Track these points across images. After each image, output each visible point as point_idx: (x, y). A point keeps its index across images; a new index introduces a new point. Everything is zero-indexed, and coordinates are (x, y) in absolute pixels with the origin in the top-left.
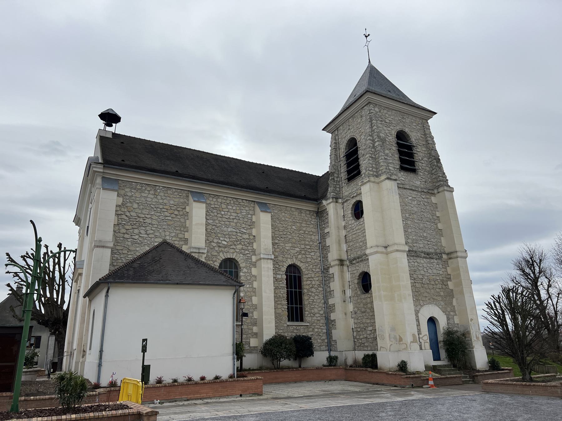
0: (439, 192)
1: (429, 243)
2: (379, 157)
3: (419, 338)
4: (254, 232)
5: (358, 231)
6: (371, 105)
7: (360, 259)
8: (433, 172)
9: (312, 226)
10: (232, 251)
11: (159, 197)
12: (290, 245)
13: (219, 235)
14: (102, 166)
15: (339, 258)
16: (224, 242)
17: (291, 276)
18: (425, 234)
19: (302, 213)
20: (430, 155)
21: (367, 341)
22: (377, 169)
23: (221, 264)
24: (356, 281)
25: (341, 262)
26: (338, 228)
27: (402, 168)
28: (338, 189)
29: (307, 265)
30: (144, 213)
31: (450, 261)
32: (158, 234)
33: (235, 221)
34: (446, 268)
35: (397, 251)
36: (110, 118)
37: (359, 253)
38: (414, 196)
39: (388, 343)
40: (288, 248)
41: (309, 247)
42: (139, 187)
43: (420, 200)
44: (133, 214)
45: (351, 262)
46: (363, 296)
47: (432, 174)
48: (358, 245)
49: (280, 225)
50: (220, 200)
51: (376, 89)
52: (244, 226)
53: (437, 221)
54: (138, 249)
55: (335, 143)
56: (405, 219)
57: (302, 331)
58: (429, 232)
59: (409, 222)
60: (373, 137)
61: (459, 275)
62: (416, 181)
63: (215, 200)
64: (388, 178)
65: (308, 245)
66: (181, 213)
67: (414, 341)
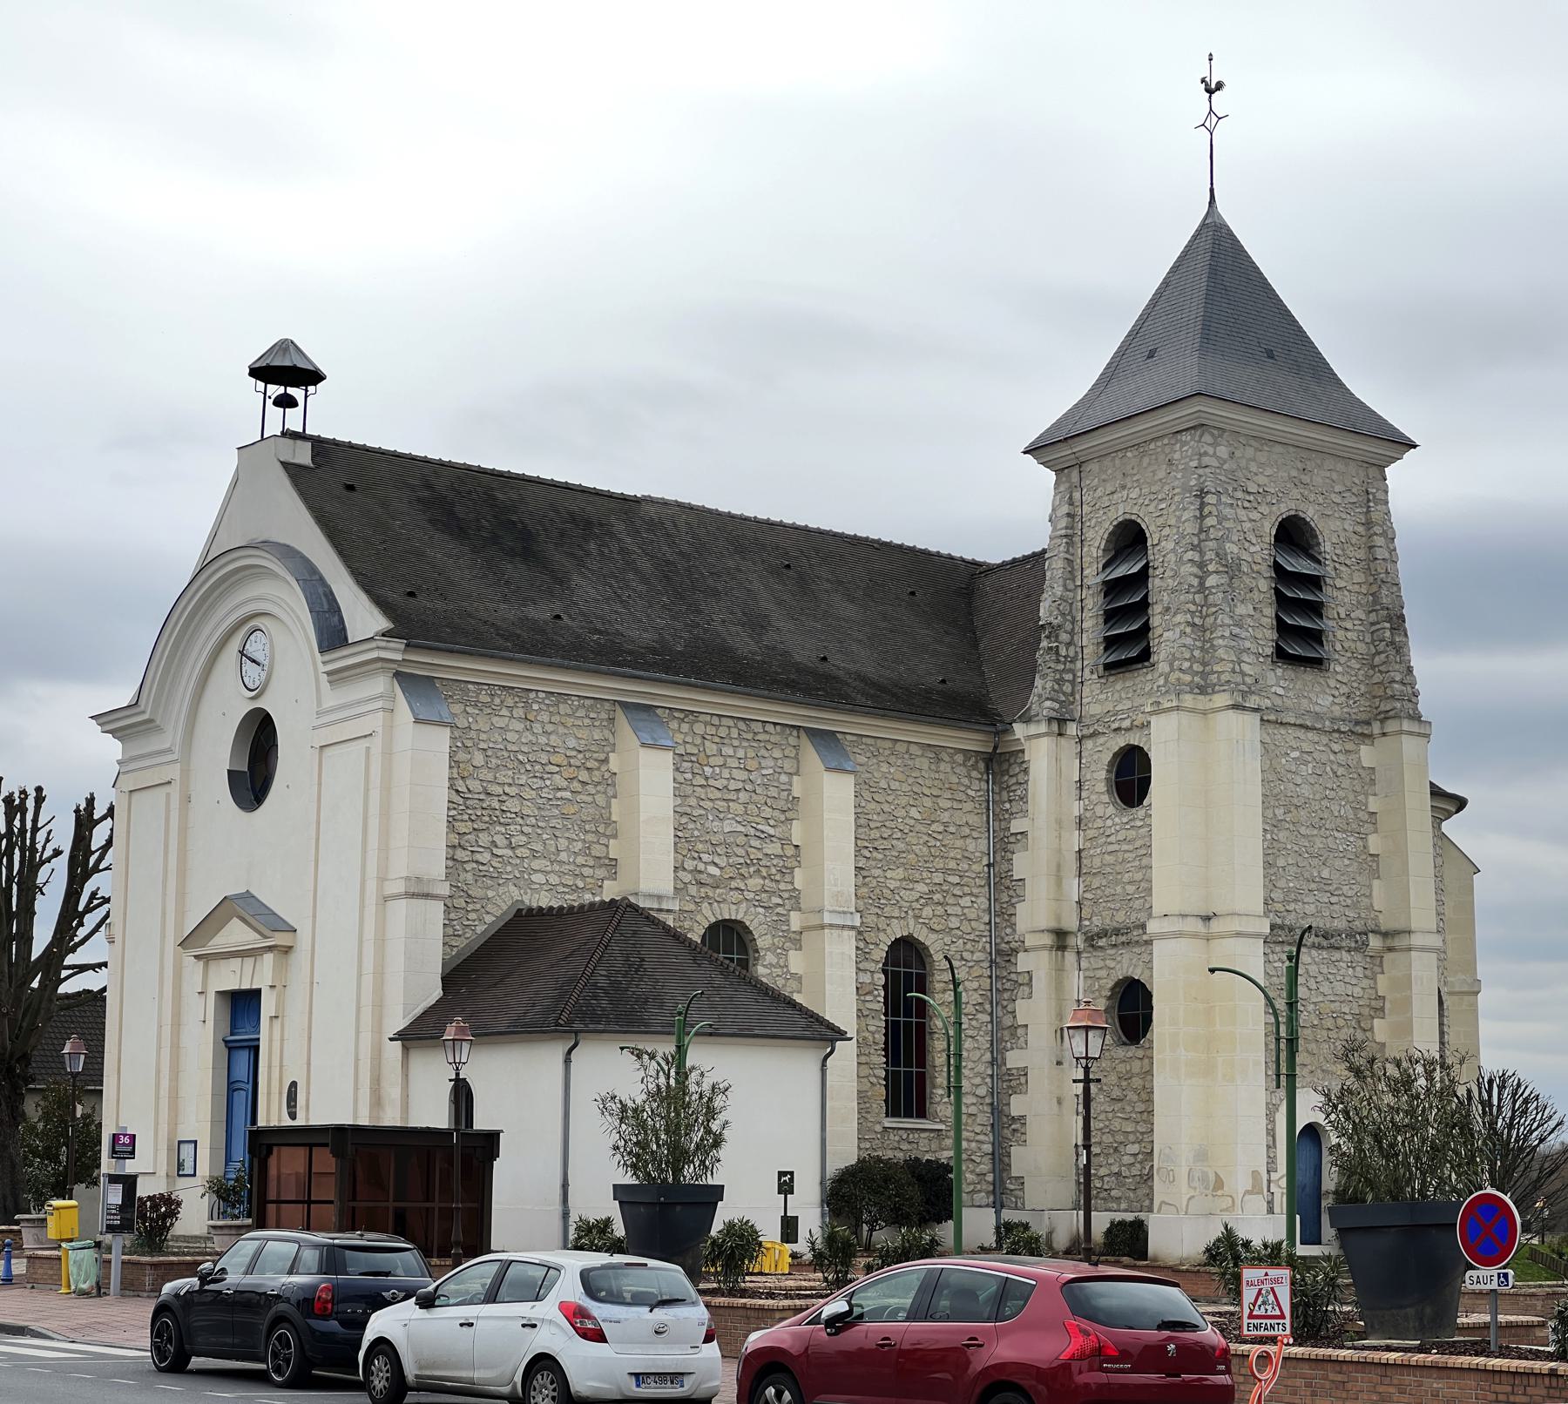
0: (1384, 734)
1: (1334, 900)
2: (1214, 627)
3: (1269, 1181)
4: (797, 833)
5: (1125, 847)
6: (1207, 438)
7: (1123, 939)
8: (1377, 660)
9: (969, 806)
10: (736, 896)
11: (537, 728)
12: (900, 873)
13: (700, 847)
14: (399, 644)
15: (1053, 924)
16: (713, 870)
17: (896, 975)
18: (1325, 874)
19: (940, 760)
20: (1375, 602)
21: (1121, 1185)
22: (1204, 664)
23: (704, 937)
24: (1101, 1005)
25: (1060, 938)
26: (1059, 822)
27: (1281, 655)
28: (1067, 688)
29: (948, 940)
30: (501, 779)
31: (1388, 957)
32: (538, 847)
33: (743, 796)
34: (1374, 979)
35: (1239, 934)
36: (286, 374)
37: (1120, 917)
38: (1306, 747)
39: (1185, 1192)
40: (893, 884)
41: (956, 880)
42: (484, 698)
43: (1324, 758)
44: (474, 785)
45: (1091, 940)
46: (1121, 1052)
47: (1373, 667)
48: (1119, 889)
49: (873, 805)
50: (699, 728)
51: (1220, 302)
52: (767, 812)
53: (1368, 827)
54: (490, 894)
55: (1068, 515)
56: (1272, 825)
57: (923, 1145)
58: (1338, 863)
59: (1282, 835)
60: (1202, 553)
61: (1408, 1001)
62: (1322, 695)
63: (685, 728)
64: (1235, 707)
65: (953, 872)
66: (597, 776)
67: (1255, 1190)
